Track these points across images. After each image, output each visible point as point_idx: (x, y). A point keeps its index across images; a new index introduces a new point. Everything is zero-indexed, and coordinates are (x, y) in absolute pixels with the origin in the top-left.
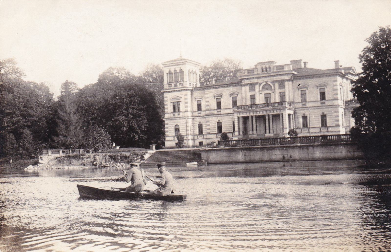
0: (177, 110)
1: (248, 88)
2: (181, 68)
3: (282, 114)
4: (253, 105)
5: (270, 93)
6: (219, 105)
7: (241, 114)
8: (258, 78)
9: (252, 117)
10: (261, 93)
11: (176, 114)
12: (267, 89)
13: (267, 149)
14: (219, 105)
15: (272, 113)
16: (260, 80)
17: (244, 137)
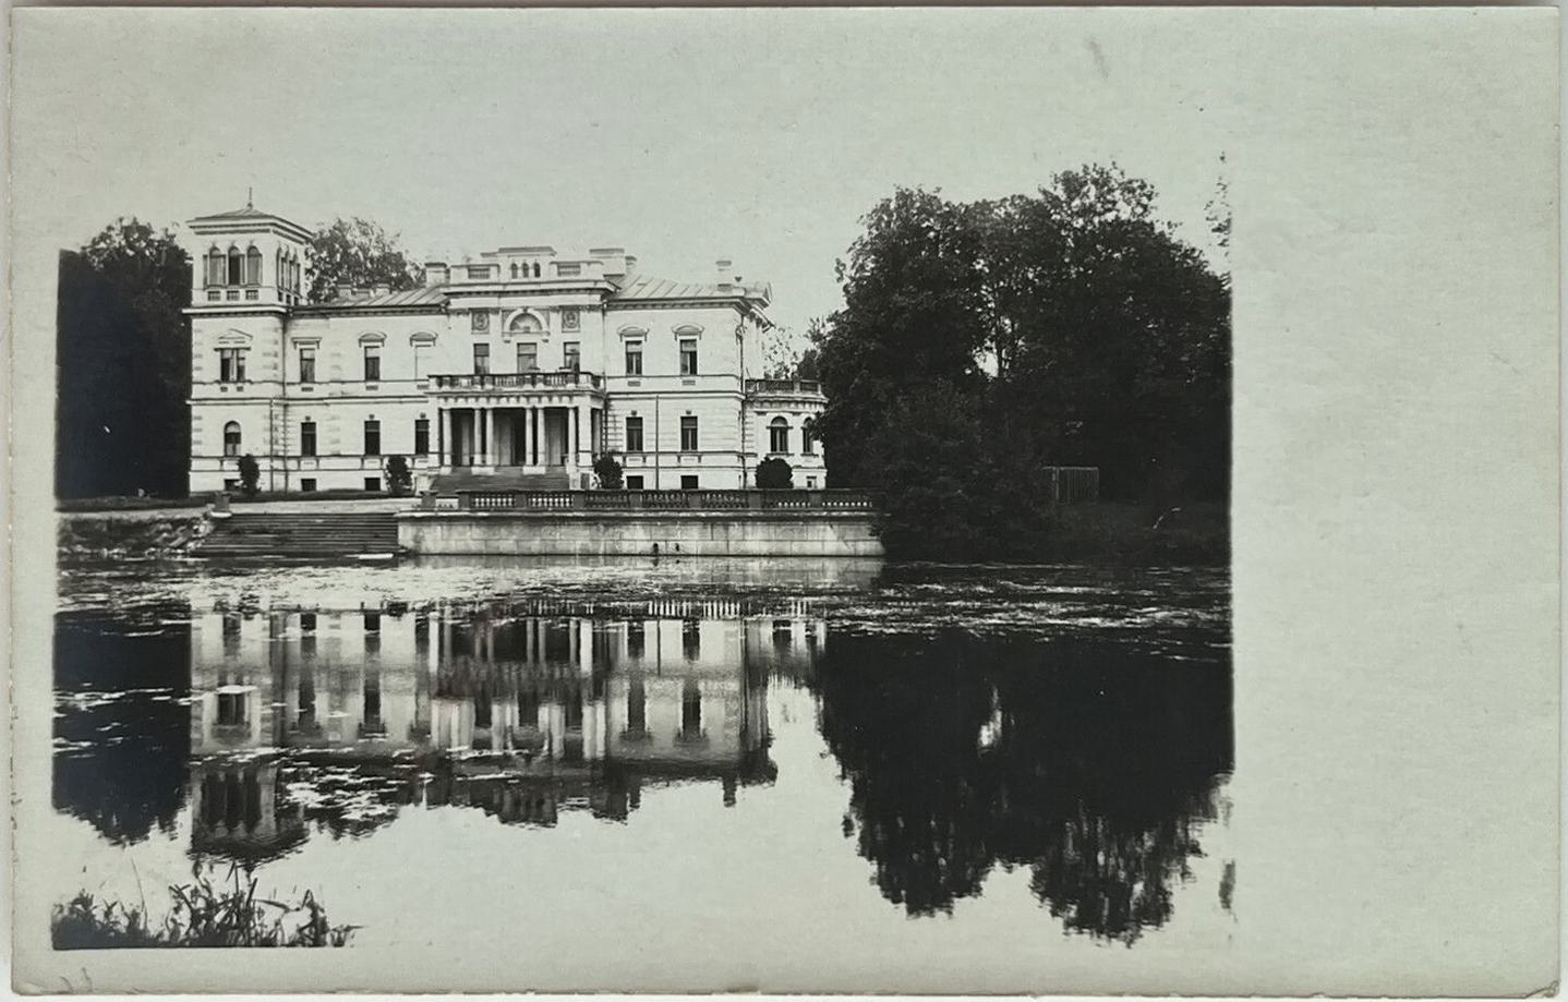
0: (233, 376)
1: (467, 320)
2: (255, 244)
3: (576, 409)
4: (481, 374)
5: (535, 344)
6: (372, 370)
7: (451, 400)
8: (501, 294)
9: (483, 411)
10: (508, 342)
11: (231, 388)
12: (527, 331)
13: (605, 522)
14: (372, 370)
15: (545, 402)
16: (505, 302)
17: (453, 471)
